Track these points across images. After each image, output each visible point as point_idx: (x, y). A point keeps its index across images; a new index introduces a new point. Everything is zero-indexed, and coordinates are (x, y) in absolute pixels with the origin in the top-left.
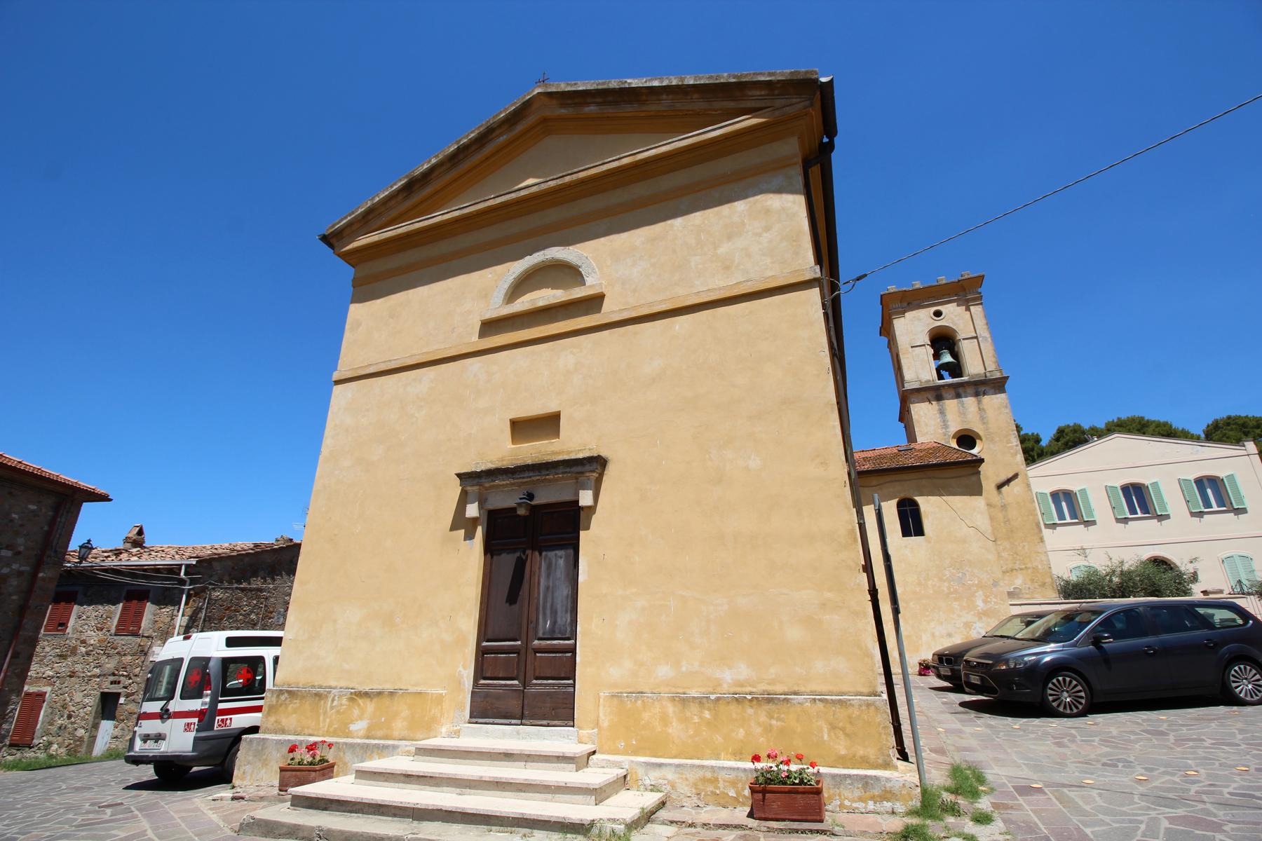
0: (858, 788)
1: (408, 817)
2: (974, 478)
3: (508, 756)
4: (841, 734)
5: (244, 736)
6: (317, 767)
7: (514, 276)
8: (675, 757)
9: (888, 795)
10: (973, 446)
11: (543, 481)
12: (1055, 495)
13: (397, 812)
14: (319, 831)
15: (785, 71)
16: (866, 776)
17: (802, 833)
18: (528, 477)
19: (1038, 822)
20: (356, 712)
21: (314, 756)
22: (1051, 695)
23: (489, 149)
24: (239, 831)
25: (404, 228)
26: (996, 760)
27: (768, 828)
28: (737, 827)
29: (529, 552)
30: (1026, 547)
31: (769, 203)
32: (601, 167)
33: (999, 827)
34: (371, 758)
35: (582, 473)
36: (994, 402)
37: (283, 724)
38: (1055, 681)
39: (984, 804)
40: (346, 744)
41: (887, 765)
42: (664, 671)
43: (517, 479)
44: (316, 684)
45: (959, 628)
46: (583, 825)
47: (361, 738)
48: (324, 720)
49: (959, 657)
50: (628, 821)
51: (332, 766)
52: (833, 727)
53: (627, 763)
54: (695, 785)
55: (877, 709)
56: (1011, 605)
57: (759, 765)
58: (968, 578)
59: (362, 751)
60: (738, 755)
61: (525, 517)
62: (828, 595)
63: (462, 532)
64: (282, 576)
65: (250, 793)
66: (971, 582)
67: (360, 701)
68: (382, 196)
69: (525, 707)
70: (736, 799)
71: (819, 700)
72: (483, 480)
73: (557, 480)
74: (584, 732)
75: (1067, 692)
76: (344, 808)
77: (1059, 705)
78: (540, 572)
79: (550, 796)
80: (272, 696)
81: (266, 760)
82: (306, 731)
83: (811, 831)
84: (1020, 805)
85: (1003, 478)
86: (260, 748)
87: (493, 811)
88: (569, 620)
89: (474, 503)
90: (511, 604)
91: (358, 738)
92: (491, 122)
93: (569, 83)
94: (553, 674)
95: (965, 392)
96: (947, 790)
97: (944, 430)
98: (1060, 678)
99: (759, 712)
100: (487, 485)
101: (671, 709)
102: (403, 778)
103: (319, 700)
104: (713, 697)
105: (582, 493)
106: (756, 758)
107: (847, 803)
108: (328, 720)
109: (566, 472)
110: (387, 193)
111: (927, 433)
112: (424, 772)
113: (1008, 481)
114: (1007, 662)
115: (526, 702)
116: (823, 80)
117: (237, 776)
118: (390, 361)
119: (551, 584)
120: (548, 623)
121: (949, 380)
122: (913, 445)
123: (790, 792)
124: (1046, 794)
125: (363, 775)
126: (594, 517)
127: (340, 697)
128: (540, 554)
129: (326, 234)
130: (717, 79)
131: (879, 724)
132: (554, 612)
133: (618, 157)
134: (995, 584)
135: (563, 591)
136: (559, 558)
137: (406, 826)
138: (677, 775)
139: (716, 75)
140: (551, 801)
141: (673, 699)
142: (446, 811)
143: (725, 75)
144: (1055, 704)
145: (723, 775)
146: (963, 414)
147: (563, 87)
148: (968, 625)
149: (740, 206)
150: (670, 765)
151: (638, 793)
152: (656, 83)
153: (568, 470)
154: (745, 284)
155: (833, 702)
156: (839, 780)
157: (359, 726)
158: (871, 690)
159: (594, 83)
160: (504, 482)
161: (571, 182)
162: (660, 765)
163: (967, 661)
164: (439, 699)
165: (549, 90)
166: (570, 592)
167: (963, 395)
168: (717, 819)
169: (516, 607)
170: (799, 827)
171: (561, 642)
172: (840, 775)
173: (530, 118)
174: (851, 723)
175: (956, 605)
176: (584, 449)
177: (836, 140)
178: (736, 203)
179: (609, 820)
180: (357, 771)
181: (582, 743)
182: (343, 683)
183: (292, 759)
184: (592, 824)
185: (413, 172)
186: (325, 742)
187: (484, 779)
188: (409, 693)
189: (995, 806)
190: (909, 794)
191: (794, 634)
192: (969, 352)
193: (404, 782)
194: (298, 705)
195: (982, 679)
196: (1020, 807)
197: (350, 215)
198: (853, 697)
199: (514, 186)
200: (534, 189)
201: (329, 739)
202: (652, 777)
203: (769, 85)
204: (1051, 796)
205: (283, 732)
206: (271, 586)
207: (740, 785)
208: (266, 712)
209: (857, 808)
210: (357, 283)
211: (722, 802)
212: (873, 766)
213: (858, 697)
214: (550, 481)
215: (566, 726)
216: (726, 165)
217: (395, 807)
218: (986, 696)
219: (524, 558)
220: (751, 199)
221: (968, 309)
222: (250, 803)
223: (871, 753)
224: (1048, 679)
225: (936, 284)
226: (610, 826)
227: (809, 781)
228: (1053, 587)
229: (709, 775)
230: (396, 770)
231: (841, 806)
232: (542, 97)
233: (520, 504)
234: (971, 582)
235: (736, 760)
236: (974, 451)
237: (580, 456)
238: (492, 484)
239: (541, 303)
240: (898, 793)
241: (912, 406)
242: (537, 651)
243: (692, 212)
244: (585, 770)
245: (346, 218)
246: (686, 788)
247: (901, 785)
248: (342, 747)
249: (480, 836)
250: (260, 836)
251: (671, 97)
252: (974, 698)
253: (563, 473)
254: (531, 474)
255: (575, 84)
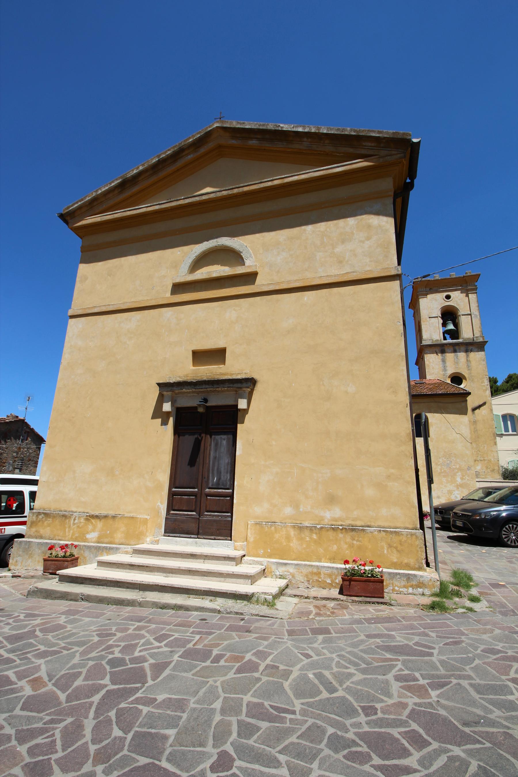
0: (404, 580)
1: (137, 589)
2: (463, 404)
3: (193, 556)
4: (395, 551)
5: (16, 539)
6: (69, 559)
7: (196, 254)
8: (294, 560)
9: (421, 585)
10: (460, 383)
11: (214, 391)
12: (505, 417)
13: (129, 586)
14: (82, 595)
15: (389, 131)
16: (409, 574)
17: (372, 603)
18: (205, 388)
19: (506, 602)
20: (90, 527)
21: (66, 552)
22: (504, 534)
23: (180, 163)
24: (27, 595)
25: (119, 214)
26: (477, 569)
27: (353, 600)
28: (334, 599)
29: (203, 435)
30: (486, 448)
31: (371, 221)
32: (259, 185)
33: (485, 604)
34: (102, 555)
35: (241, 388)
36: (477, 356)
37: (41, 533)
38: (507, 526)
39: (474, 592)
40: (85, 546)
41: (420, 569)
42: (288, 511)
43: (198, 389)
44: (63, 509)
45: (444, 494)
46: (248, 595)
47: (94, 543)
48: (69, 531)
49: (448, 510)
50: (274, 594)
51: (77, 559)
52: (390, 546)
53: (265, 562)
54: (307, 576)
55: (417, 537)
56: (477, 481)
57: (347, 566)
58: (453, 465)
59: (95, 551)
60: (333, 560)
61: (202, 414)
62: (392, 471)
63: (159, 420)
64: (11, 440)
65: (24, 574)
66: (454, 467)
67: (93, 521)
68: (103, 190)
69: (200, 528)
70: (331, 584)
71: (383, 531)
72: (175, 388)
73: (223, 391)
74: (238, 544)
75: (514, 533)
76: (94, 583)
77: (508, 541)
78: (210, 448)
79: (223, 579)
80: (33, 516)
81: (31, 554)
82: (57, 538)
83: (378, 603)
84: (494, 593)
85: (477, 404)
86: (27, 547)
87: (191, 586)
88: (229, 478)
89: (168, 402)
90: (191, 466)
91: (92, 542)
92: (183, 144)
93: (239, 122)
94: (187, 509)
95: (460, 349)
96: (452, 583)
97: (444, 372)
98: (511, 525)
99: (346, 536)
100: (177, 392)
101: (292, 533)
102: (129, 567)
103: (65, 519)
104: (318, 526)
105: (240, 400)
106: (346, 562)
107: (397, 588)
108: (71, 532)
109: (230, 387)
110: (107, 188)
111: (433, 373)
112: (143, 564)
113: (479, 407)
114: (480, 514)
115: (200, 525)
116: (415, 140)
117: (12, 563)
118: (109, 305)
119: (217, 456)
120: (215, 479)
121: (449, 341)
122: (424, 381)
123: (366, 581)
124: (507, 588)
125: (102, 564)
126: (247, 416)
127: (79, 518)
128: (211, 437)
129: (63, 213)
130: (342, 131)
131: (418, 545)
132: (219, 473)
133: (271, 179)
134: (469, 468)
135: (225, 460)
136: (224, 440)
137: (136, 594)
138: (296, 570)
139: (342, 128)
140: (224, 582)
141: (294, 527)
142: (161, 586)
143: (349, 129)
144: (506, 540)
145: (323, 571)
146: (456, 363)
147: (235, 124)
148: (450, 492)
149: (351, 221)
150: (292, 564)
151: (272, 579)
152: (300, 129)
153: (231, 385)
154: (352, 274)
155: (391, 532)
156: (393, 576)
157: (92, 536)
158: (414, 526)
159: (257, 124)
160: (188, 391)
161: (238, 193)
162: (286, 564)
163: (455, 513)
164: (145, 522)
165: (225, 126)
166: (230, 461)
167: (458, 351)
168: (321, 595)
169: (195, 468)
170: (371, 600)
171: (224, 491)
172: (394, 573)
173: (210, 144)
174: (401, 544)
175: (444, 480)
176: (242, 373)
177: (416, 181)
178: (349, 219)
179: (262, 593)
180: (98, 562)
181: (237, 550)
182: (81, 510)
183: (51, 554)
184: (253, 595)
185: (126, 174)
186: (73, 544)
187: (181, 569)
188: (125, 517)
189: (480, 593)
190: (433, 585)
191: (370, 492)
192: (464, 323)
193: (129, 569)
194: (51, 522)
195: (464, 524)
196: (494, 594)
197: (80, 201)
198: (403, 530)
199: (194, 193)
200: (212, 196)
201: (76, 543)
202: (281, 570)
203: (377, 139)
204: (511, 589)
205: (41, 537)
206: (4, 446)
207: (334, 577)
208: (29, 526)
209: (403, 591)
210: (84, 249)
211: (323, 585)
212: (412, 568)
213: (406, 530)
214: (218, 391)
215: (226, 540)
216: (343, 192)
217: (128, 583)
218: (465, 533)
219: (200, 438)
220: (359, 217)
221: (467, 296)
222: (25, 579)
223: (412, 561)
224: (504, 525)
225: (449, 277)
226: (263, 596)
227: (377, 575)
228: (499, 472)
229: (315, 570)
230: (124, 562)
231: (393, 590)
232: (218, 130)
233: (200, 405)
234: (454, 467)
235: (331, 563)
236: (462, 386)
237: (239, 377)
238: (180, 391)
239: (215, 275)
240: (427, 584)
241: (425, 355)
242: (208, 495)
243: (319, 222)
244: (240, 565)
245: (77, 203)
246: (301, 577)
247: (429, 580)
248: (83, 548)
249: (185, 600)
250: (42, 598)
251: (309, 140)
252: (455, 534)
253: (228, 387)
254: (207, 386)
255: (243, 123)
